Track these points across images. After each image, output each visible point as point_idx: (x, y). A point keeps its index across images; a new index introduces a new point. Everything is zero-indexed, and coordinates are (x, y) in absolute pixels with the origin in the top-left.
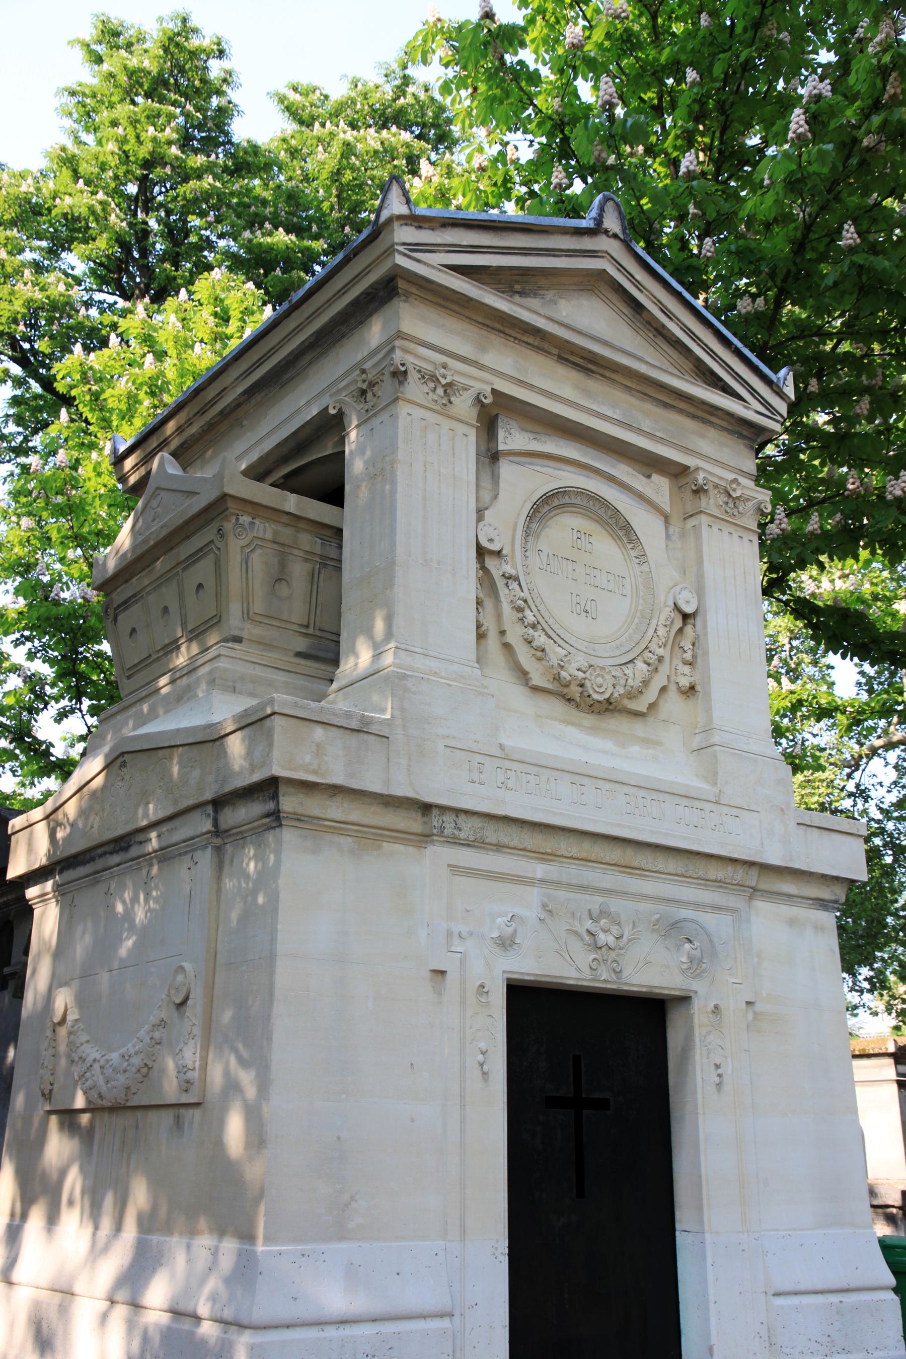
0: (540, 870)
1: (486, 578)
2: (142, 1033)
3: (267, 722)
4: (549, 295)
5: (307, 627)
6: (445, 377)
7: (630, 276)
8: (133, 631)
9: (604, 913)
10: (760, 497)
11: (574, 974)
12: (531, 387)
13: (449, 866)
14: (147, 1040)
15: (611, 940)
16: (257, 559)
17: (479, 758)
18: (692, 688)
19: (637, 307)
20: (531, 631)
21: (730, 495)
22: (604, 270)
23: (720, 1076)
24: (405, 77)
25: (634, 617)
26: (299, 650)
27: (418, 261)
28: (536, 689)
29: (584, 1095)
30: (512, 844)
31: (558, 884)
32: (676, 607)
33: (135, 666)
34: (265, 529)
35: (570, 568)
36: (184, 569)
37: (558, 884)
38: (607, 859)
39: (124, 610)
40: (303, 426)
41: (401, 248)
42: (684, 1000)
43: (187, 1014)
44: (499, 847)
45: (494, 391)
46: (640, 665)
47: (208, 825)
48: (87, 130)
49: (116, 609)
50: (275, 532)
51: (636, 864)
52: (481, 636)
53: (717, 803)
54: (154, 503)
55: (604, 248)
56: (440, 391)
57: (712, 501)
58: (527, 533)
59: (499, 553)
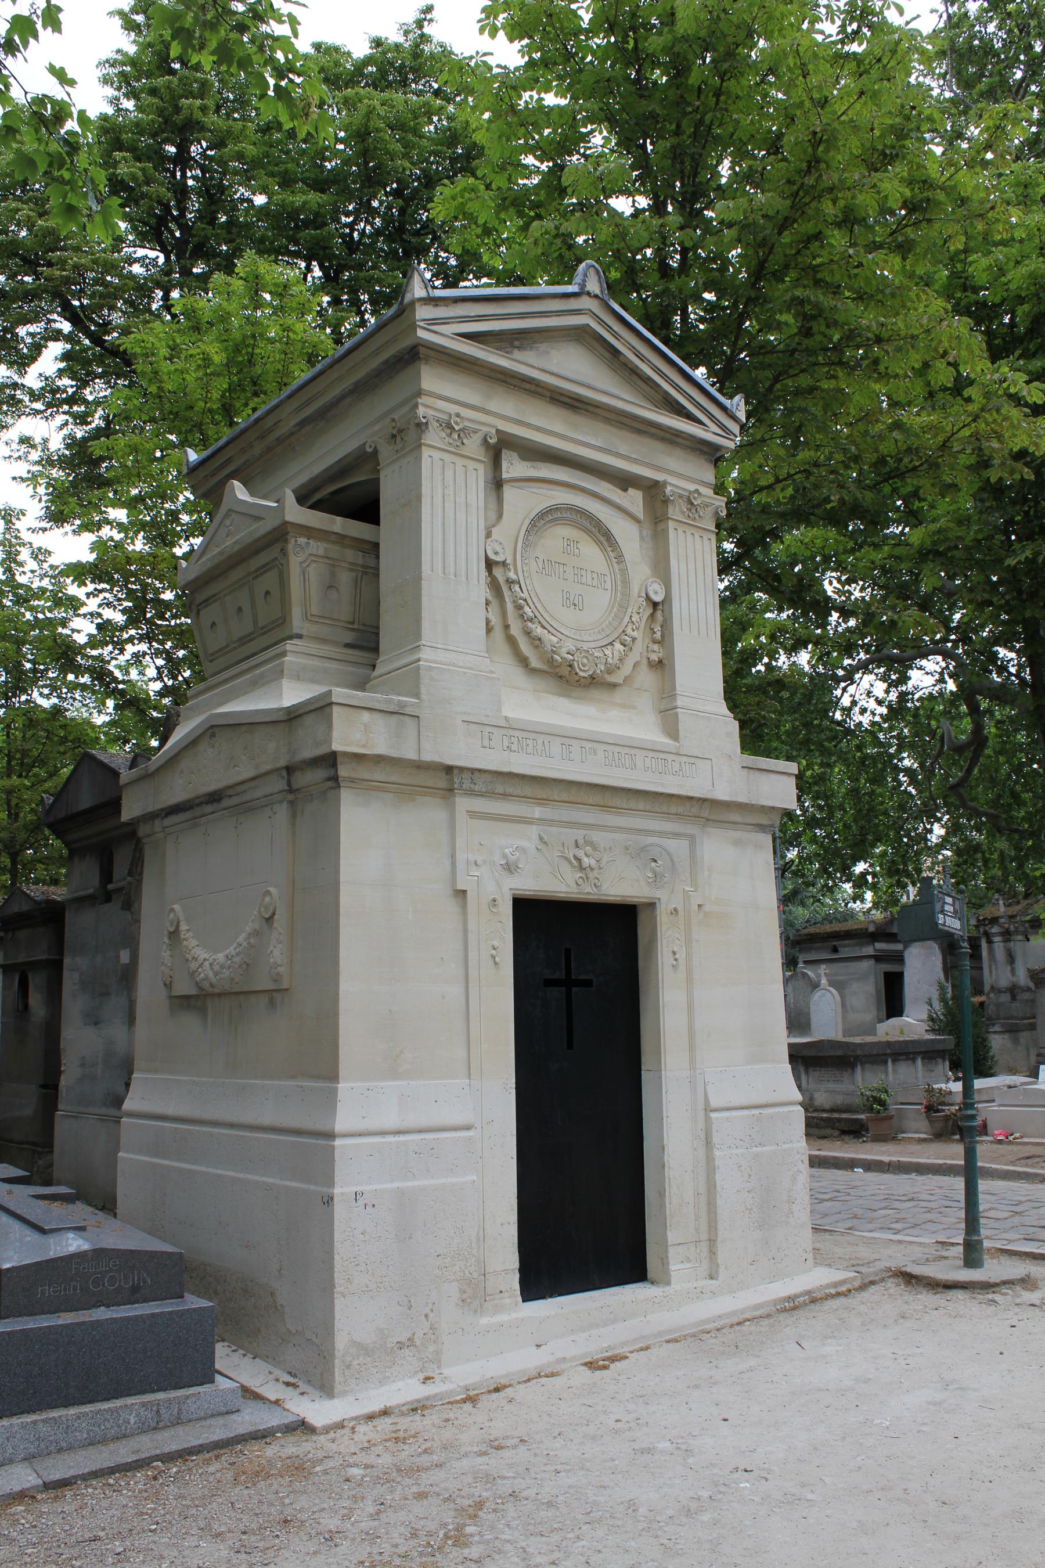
0: (537, 812)
1: (494, 586)
2: (241, 939)
3: (327, 709)
4: (543, 347)
5: (353, 623)
6: (457, 423)
7: (609, 329)
8: (214, 624)
9: (588, 843)
10: (717, 503)
11: (564, 889)
12: (528, 426)
13: (467, 811)
14: (245, 944)
15: (593, 862)
16: (313, 571)
17: (489, 729)
18: (660, 662)
19: (615, 352)
20: (530, 624)
21: (692, 504)
22: (588, 325)
23: (676, 960)
24: (423, 35)
25: (613, 607)
26: (347, 641)
27: (435, 332)
28: (533, 671)
29: (573, 977)
30: (515, 793)
31: (550, 822)
32: (648, 598)
33: (217, 652)
34: (318, 547)
35: (561, 570)
36: (255, 578)
37: (550, 822)
38: (591, 801)
39: (205, 607)
40: (345, 457)
41: (422, 324)
42: (652, 905)
43: (275, 925)
44: (505, 796)
45: (498, 431)
46: (618, 646)
47: (282, 785)
48: (127, 96)
49: (198, 605)
50: (326, 549)
51: (614, 804)
52: (489, 630)
53: (677, 754)
54: (228, 522)
55: (587, 307)
56: (455, 436)
57: (677, 509)
58: (527, 544)
59: (504, 564)
